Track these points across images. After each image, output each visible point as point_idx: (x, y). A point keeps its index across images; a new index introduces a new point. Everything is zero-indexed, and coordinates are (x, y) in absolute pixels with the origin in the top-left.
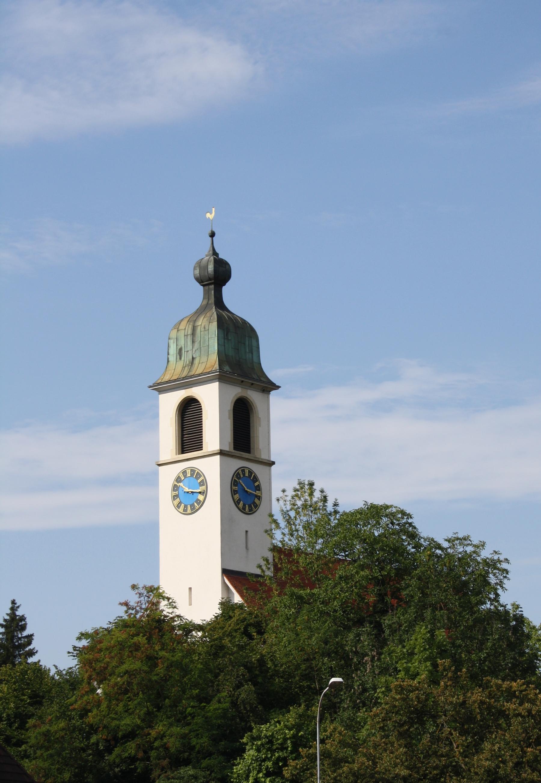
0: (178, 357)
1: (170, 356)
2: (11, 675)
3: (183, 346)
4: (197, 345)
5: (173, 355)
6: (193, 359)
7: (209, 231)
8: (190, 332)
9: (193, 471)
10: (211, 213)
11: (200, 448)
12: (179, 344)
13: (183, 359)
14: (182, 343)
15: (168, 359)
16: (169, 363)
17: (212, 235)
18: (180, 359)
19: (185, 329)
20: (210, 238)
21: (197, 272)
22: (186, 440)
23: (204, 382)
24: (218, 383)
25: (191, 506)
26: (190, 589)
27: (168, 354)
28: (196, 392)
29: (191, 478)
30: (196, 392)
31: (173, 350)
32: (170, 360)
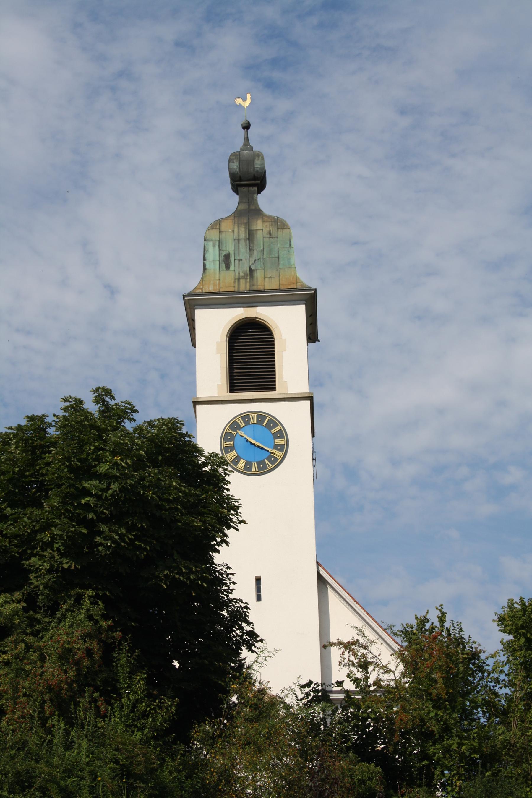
0: (223, 265)
1: (207, 263)
2: (322, 780)
3: (232, 253)
4: (256, 255)
5: (214, 261)
6: (251, 271)
7: (243, 121)
8: (243, 235)
9: (261, 416)
10: (245, 100)
11: (273, 388)
12: (224, 249)
13: (232, 268)
14: (230, 247)
15: (204, 265)
16: (207, 271)
17: (247, 127)
18: (228, 267)
19: (233, 231)
20: (243, 131)
21: (235, 166)
22: (236, 376)
23: (280, 301)
24: (196, 311)
25: (259, 463)
26: (258, 580)
27: (205, 259)
28: (265, 313)
29: (259, 426)
30: (265, 313)
31: (213, 254)
32: (207, 267)
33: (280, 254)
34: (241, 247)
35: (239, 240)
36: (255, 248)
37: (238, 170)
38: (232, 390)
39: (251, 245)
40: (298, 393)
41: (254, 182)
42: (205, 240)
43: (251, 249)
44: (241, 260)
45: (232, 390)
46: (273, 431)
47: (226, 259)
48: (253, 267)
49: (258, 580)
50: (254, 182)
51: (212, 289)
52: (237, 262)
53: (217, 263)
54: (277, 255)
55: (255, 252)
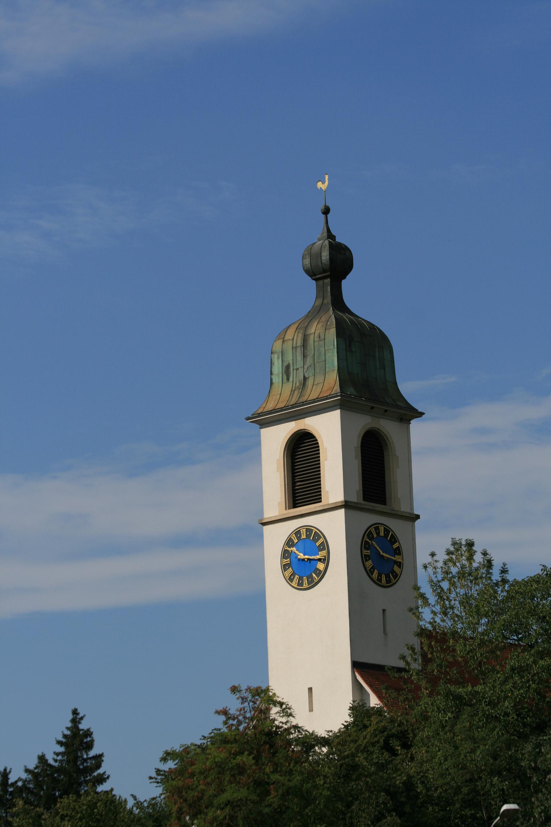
0: (285, 377)
1: (273, 377)
3: (291, 362)
5: (278, 374)
6: (305, 379)
11: (318, 500)
12: (285, 360)
13: (291, 379)
15: (271, 380)
16: (273, 385)
17: (326, 211)
18: (288, 379)
20: (323, 216)
21: (307, 261)
23: (318, 410)
26: (310, 689)
31: (277, 368)
32: (274, 381)
33: (327, 357)
34: (298, 355)
35: (296, 347)
36: (308, 354)
37: (309, 265)
38: (295, 505)
39: (305, 351)
40: (336, 503)
41: (325, 274)
42: (272, 353)
43: (304, 356)
44: (298, 369)
45: (365, 499)
46: (318, 544)
47: (287, 370)
48: (307, 376)
49: (310, 689)
50: (325, 274)
51: (313, 396)
52: (295, 371)
53: (281, 375)
54: (324, 358)
55: (308, 359)
